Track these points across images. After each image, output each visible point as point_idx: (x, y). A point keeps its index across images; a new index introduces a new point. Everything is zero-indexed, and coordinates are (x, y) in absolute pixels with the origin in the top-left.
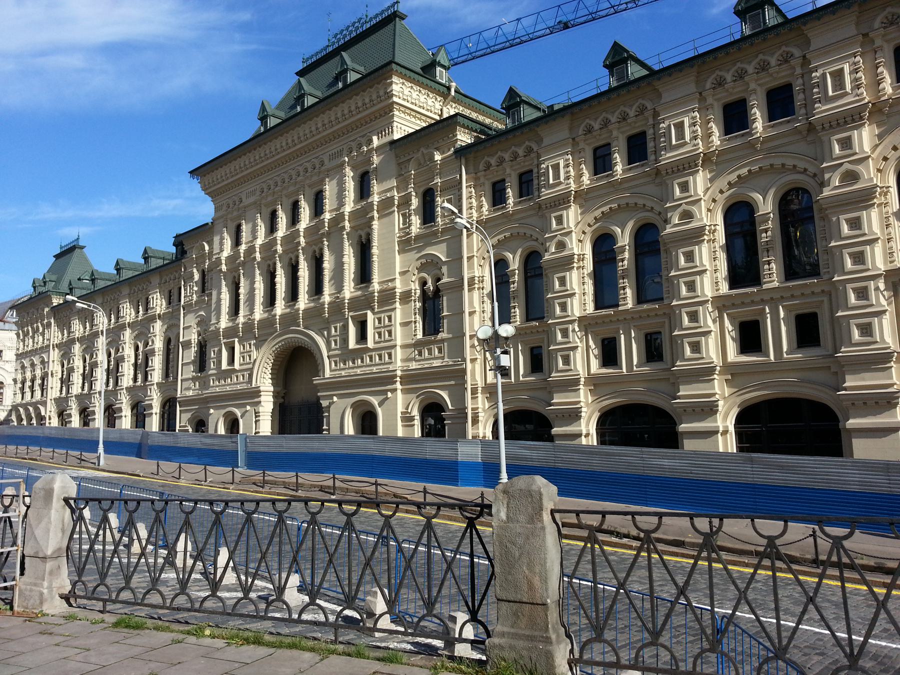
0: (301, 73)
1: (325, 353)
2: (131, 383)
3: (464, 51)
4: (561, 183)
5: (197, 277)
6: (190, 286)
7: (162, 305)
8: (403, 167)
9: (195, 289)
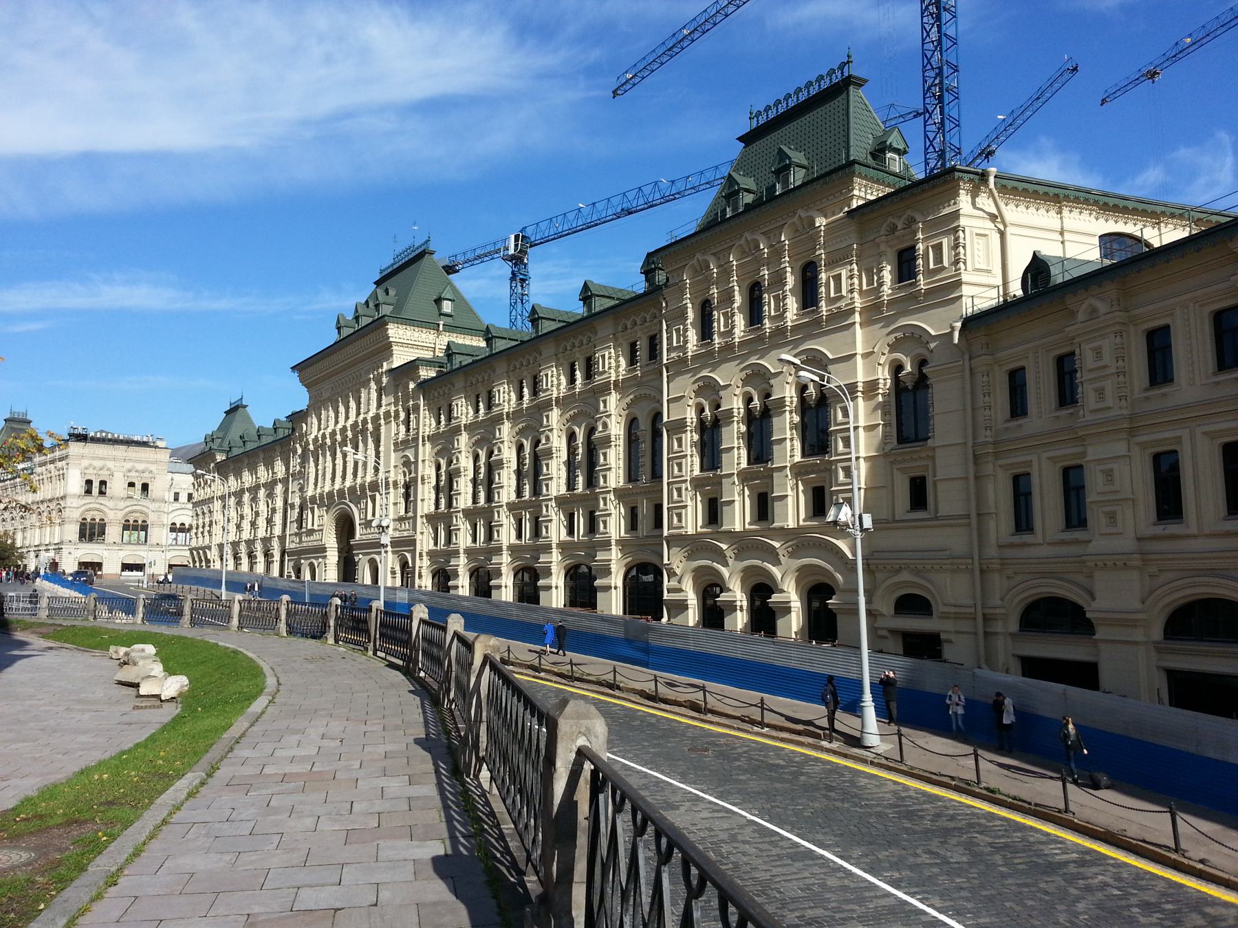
0: (378, 283)
1: (357, 522)
2: (513, 497)
3: (610, 212)
4: (842, 297)
5: (299, 451)
6: (678, 331)
7: (467, 413)
8: (772, 235)
9: (299, 461)
